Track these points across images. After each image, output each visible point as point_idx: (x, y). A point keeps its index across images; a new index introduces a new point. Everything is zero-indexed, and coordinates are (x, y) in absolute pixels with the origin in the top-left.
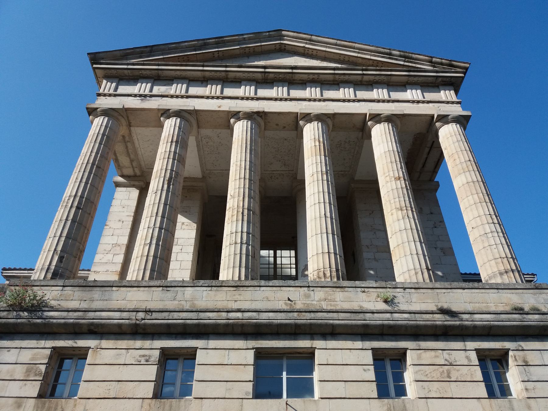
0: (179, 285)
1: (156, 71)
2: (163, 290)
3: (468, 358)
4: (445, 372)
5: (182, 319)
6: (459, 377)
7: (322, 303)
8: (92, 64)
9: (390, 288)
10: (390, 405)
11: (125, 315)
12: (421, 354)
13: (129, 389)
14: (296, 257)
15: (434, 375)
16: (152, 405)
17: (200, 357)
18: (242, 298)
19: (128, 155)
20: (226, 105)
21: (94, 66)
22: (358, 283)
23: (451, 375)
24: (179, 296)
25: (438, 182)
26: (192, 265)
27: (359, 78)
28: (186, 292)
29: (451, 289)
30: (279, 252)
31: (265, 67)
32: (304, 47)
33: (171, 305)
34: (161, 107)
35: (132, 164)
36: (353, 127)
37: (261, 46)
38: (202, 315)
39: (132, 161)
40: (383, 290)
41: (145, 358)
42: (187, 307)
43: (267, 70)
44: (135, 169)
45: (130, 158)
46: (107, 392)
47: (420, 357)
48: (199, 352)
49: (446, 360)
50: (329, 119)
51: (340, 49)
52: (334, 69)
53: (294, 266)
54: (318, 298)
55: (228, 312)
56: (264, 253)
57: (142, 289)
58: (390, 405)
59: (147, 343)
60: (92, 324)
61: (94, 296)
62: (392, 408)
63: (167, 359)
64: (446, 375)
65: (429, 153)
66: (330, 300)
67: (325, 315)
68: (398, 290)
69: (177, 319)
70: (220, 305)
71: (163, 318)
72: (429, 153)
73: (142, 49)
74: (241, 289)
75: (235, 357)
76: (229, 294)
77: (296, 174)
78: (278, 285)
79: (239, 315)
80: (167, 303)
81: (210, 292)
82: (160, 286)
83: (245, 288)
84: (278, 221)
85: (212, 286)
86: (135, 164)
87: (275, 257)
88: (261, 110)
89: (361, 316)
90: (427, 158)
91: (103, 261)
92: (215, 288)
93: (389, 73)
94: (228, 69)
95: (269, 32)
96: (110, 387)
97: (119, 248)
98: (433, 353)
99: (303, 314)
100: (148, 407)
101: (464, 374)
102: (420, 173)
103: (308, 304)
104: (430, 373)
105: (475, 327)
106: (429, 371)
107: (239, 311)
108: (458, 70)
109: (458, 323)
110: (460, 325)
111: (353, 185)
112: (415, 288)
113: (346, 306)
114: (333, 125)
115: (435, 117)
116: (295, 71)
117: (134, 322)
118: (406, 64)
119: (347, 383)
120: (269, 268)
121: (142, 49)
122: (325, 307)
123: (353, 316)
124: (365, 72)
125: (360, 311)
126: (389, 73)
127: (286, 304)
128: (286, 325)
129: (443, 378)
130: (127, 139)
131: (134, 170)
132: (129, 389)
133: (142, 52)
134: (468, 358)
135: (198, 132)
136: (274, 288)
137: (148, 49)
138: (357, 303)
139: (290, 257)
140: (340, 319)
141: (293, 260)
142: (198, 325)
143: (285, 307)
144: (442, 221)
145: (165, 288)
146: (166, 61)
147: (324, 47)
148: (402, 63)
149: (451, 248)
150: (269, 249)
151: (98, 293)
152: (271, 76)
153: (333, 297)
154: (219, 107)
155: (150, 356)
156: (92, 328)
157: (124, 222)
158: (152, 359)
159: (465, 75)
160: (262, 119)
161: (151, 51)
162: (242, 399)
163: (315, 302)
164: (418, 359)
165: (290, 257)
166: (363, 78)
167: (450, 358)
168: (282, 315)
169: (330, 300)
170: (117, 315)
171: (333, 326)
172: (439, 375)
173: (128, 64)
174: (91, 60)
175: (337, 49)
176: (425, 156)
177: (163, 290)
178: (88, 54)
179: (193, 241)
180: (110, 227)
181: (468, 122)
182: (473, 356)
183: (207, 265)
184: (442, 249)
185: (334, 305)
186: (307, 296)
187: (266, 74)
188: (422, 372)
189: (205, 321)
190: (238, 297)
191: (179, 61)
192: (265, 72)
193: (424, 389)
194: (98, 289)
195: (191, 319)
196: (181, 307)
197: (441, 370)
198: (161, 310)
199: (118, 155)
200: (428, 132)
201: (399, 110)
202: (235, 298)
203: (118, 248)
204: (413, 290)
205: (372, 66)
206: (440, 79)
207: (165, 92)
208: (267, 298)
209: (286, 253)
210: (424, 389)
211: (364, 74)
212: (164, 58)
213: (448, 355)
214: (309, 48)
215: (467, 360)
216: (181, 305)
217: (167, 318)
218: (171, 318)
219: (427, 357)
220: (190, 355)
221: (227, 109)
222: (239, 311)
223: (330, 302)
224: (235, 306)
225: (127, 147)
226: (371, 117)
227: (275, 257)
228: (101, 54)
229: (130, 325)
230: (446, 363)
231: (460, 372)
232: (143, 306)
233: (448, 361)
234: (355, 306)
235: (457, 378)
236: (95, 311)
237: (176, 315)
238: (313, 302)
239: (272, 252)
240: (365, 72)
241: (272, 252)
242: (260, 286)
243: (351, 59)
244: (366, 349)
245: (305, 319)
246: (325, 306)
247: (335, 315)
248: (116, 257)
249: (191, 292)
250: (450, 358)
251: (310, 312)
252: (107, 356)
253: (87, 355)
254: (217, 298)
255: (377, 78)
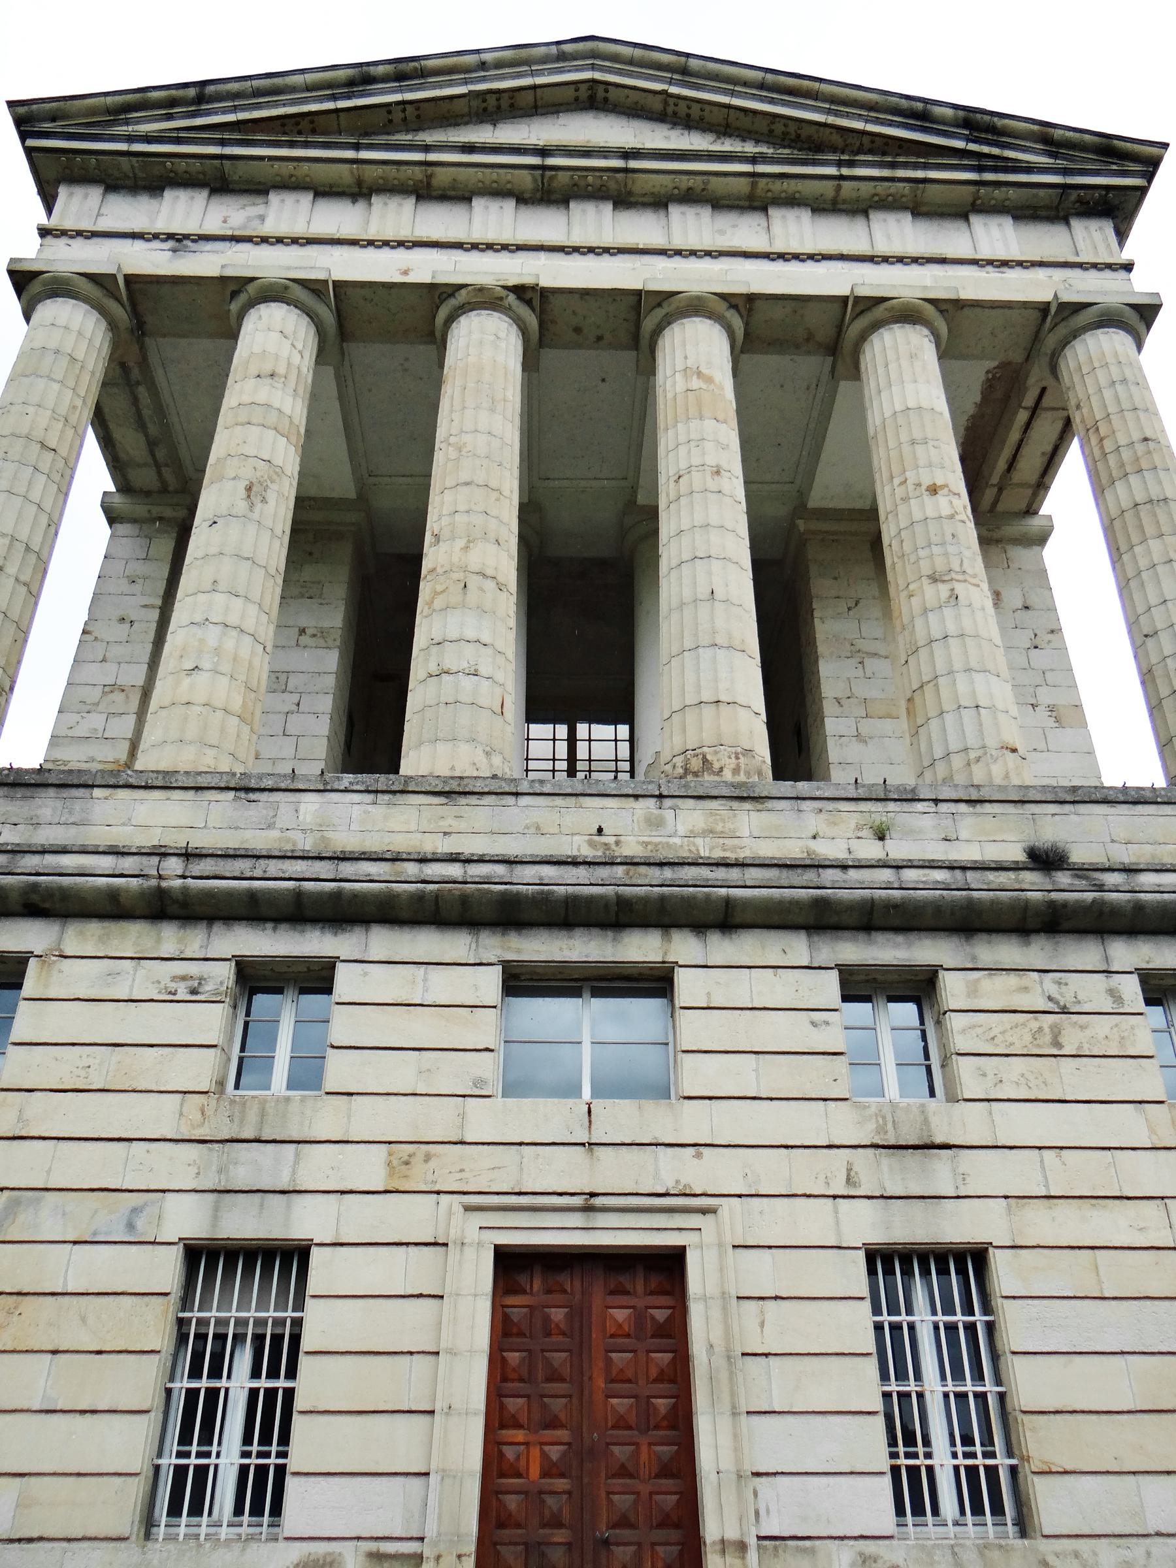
0: (283, 786)
1: (217, 162)
2: (236, 798)
3: (1113, 993)
4: (1047, 1030)
5: (290, 879)
6: (1086, 1046)
7: (699, 841)
8: (23, 136)
9: (895, 800)
10: (884, 1118)
11: (128, 864)
12: (978, 980)
13: (146, 1067)
14: (632, 740)
15: (1015, 1039)
16: (209, 1112)
17: (346, 981)
18: (462, 825)
19: (141, 425)
20: (424, 268)
21: (31, 142)
22: (803, 787)
23: (1061, 1040)
24: (285, 817)
25: (1050, 517)
26: (330, 747)
27: (828, 188)
28: (302, 807)
29: (1074, 802)
30: (582, 729)
31: (543, 152)
32: (664, 92)
33: (259, 841)
34: (229, 272)
35: (153, 455)
36: (808, 340)
37: (535, 87)
38: (347, 869)
39: (152, 445)
40: (879, 806)
41: (190, 983)
42: (307, 844)
43: (551, 161)
44: (164, 470)
45: (146, 435)
46: (83, 1073)
47: (976, 991)
48: (341, 971)
49: (1050, 998)
50: (732, 311)
51: (772, 101)
52: (753, 160)
53: (626, 766)
54: (687, 828)
55: (423, 860)
56: (537, 730)
57: (177, 795)
58: (884, 1118)
59: (194, 940)
60: (35, 887)
61: (40, 812)
62: (890, 1126)
63: (253, 991)
64: (1048, 1038)
65: (1028, 426)
66: (722, 835)
67: (705, 872)
68: (920, 806)
69: (277, 879)
70: (400, 844)
71: (237, 874)
72: (1028, 426)
73: (173, 92)
74: (463, 800)
75: (443, 985)
76: (427, 813)
77: (634, 490)
78: (569, 791)
79: (454, 871)
80: (248, 834)
81: (370, 808)
82: (228, 789)
83: (473, 800)
84: (584, 635)
85: (377, 792)
86: (161, 454)
87: (572, 740)
88: (528, 280)
89: (810, 876)
90: (1021, 441)
91: (77, 732)
92: (387, 797)
93: (920, 174)
94: (433, 157)
95: (558, 43)
96: (91, 1061)
97: (122, 696)
98: (1012, 980)
99: (643, 869)
100: (199, 1115)
101: (1101, 1036)
102: (1000, 490)
103: (656, 845)
104: (1003, 1033)
105: (1139, 907)
106: (1000, 1029)
107: (453, 858)
108: (1133, 167)
109: (1089, 896)
110: (1094, 901)
111: (801, 525)
112: (967, 801)
113: (768, 850)
114: (747, 334)
115: (1053, 310)
116: (633, 164)
117: (153, 882)
118: (973, 147)
119: (761, 1056)
120: (554, 771)
121: (173, 92)
122: (704, 853)
123: (786, 877)
124: (845, 171)
125: (808, 862)
126: (920, 174)
127: (591, 844)
128: (590, 900)
129: (1039, 1046)
130: (136, 374)
131: (159, 473)
132: (146, 1067)
133: (172, 103)
134: (1113, 993)
135: (343, 354)
136: (559, 801)
137: (192, 92)
138: (800, 843)
139: (616, 740)
140: (748, 884)
141: (624, 750)
142: (337, 895)
143: (587, 852)
144: (1055, 631)
145: (242, 795)
146: (246, 133)
147: (725, 92)
148: (959, 144)
149: (1078, 707)
150: (555, 721)
151: (50, 802)
152: (563, 177)
153: (729, 825)
154: (406, 273)
155: (201, 980)
156: (35, 898)
157: (136, 625)
158: (208, 987)
159: (1150, 181)
160: (533, 310)
161: (200, 99)
162: (464, 1096)
163: (677, 841)
164: (968, 996)
165: (616, 740)
166: (839, 188)
167: (1061, 994)
168: (581, 873)
169: (722, 835)
170: (106, 863)
171: (728, 902)
172: (1028, 1038)
173: (130, 139)
174: (19, 122)
175: (762, 99)
176: (1014, 436)
177: (236, 798)
178: (11, 104)
179: (330, 681)
180: (96, 638)
181: (1149, 326)
182: (1131, 988)
183: (370, 736)
184: (1051, 709)
185: (734, 849)
186: (656, 823)
187: (548, 173)
188: (979, 1031)
189: (357, 886)
190: (454, 823)
191: (285, 133)
192: (544, 168)
193: (984, 1075)
194: (51, 792)
195: (319, 879)
196: (289, 847)
197: (1034, 1025)
198: (231, 852)
199: (112, 426)
200: (1027, 358)
201: (947, 288)
202: (444, 825)
203: (118, 697)
204: (963, 807)
205: (870, 152)
206: (1074, 195)
207: (244, 227)
208: (538, 828)
209: (603, 731)
210: (984, 1075)
211: (842, 177)
212: (239, 122)
213: (1056, 987)
214: (678, 97)
215: (1110, 1000)
216: (288, 840)
217: (248, 875)
218: (258, 873)
219: (996, 990)
220: (317, 978)
221: (427, 280)
222: (453, 858)
223: (721, 841)
224: (445, 846)
225: (135, 401)
226: (858, 309)
227: (572, 740)
228: (979, 116)
229: (142, 894)
230: (1050, 1006)
231: (1088, 1032)
232: (178, 840)
233: (1057, 1003)
234: (793, 850)
235: (1079, 1048)
236: (43, 852)
237: (274, 868)
238: (672, 840)
239: (562, 730)
240: (845, 171)
241: (562, 730)
242: (517, 794)
243: (807, 131)
244: (820, 968)
245: (646, 884)
246: (705, 849)
247: (734, 874)
248: (114, 721)
249: (317, 806)
250: (1061, 994)
251: (661, 864)
252: (78, 977)
253: (22, 974)
254: (392, 825)
255: (881, 188)
